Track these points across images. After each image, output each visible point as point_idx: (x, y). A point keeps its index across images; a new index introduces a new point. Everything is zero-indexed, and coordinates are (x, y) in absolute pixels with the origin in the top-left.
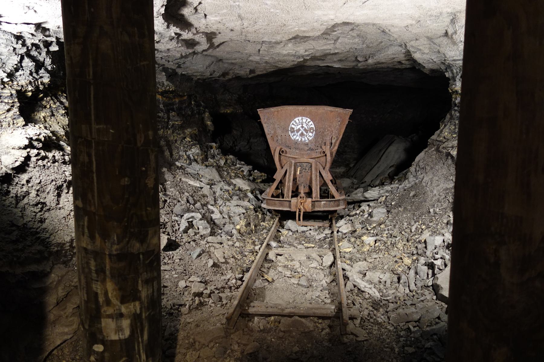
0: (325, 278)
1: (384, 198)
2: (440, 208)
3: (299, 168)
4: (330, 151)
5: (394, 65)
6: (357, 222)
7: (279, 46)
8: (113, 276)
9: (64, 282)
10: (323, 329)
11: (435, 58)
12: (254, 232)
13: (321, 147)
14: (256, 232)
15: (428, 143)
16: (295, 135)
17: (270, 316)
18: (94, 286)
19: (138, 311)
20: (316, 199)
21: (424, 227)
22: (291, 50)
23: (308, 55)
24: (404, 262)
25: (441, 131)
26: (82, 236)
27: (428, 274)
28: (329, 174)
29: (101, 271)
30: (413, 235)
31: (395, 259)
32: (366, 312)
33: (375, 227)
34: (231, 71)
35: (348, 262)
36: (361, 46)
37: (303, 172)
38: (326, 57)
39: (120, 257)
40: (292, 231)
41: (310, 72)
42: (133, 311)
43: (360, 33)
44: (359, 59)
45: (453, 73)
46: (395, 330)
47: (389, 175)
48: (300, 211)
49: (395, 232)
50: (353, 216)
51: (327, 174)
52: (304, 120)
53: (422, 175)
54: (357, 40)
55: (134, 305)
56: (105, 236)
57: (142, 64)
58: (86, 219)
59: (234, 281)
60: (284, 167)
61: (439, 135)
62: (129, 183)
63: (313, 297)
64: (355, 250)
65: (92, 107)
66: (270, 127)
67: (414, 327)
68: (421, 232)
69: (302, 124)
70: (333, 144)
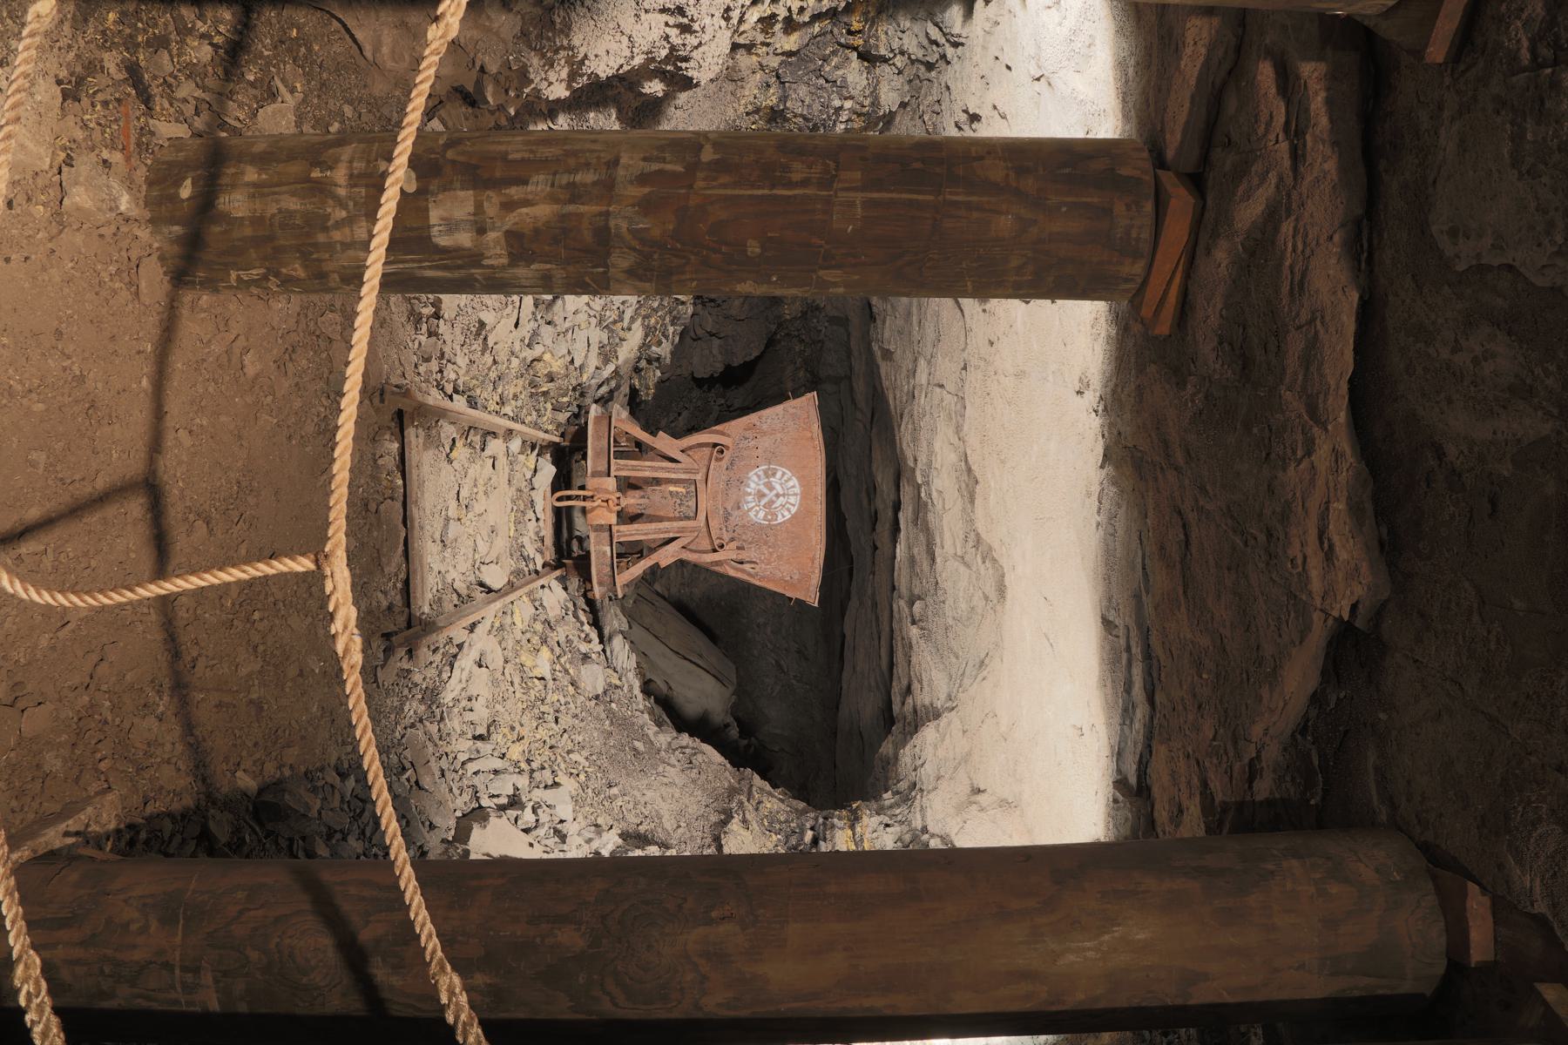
1: (618, 683)
2: (623, 808)
3: (684, 490)
4: (726, 561)
5: (899, 678)
8: (563, 217)
9: (484, 39)
10: (385, 593)
11: (928, 771)
12: (533, 390)
13: (732, 540)
15: (742, 769)
16: (760, 479)
17: (404, 478)
18: (542, 177)
19: (485, 262)
20: (615, 535)
21: (582, 777)
24: (513, 746)
25: (770, 794)
26: (642, 155)
27: (498, 796)
29: (575, 194)
30: (563, 758)
31: (517, 725)
32: (417, 678)
33: (567, 671)
34: (889, 306)
35: (497, 625)
36: (950, 614)
38: (922, 531)
39: (604, 236)
41: (879, 480)
42: (488, 254)
44: (918, 606)
45: (891, 807)
46: (395, 741)
48: (585, 498)
49: (566, 720)
51: (673, 556)
52: (792, 500)
53: (676, 763)
55: (500, 256)
56: (647, 206)
57: (969, 283)
58: (679, 168)
59: (453, 376)
60: (684, 455)
61: (762, 790)
62: (749, 253)
64: (519, 636)
65: (894, 195)
66: (775, 421)
67: (408, 780)
68: (571, 774)
69: (784, 495)
70: (740, 566)
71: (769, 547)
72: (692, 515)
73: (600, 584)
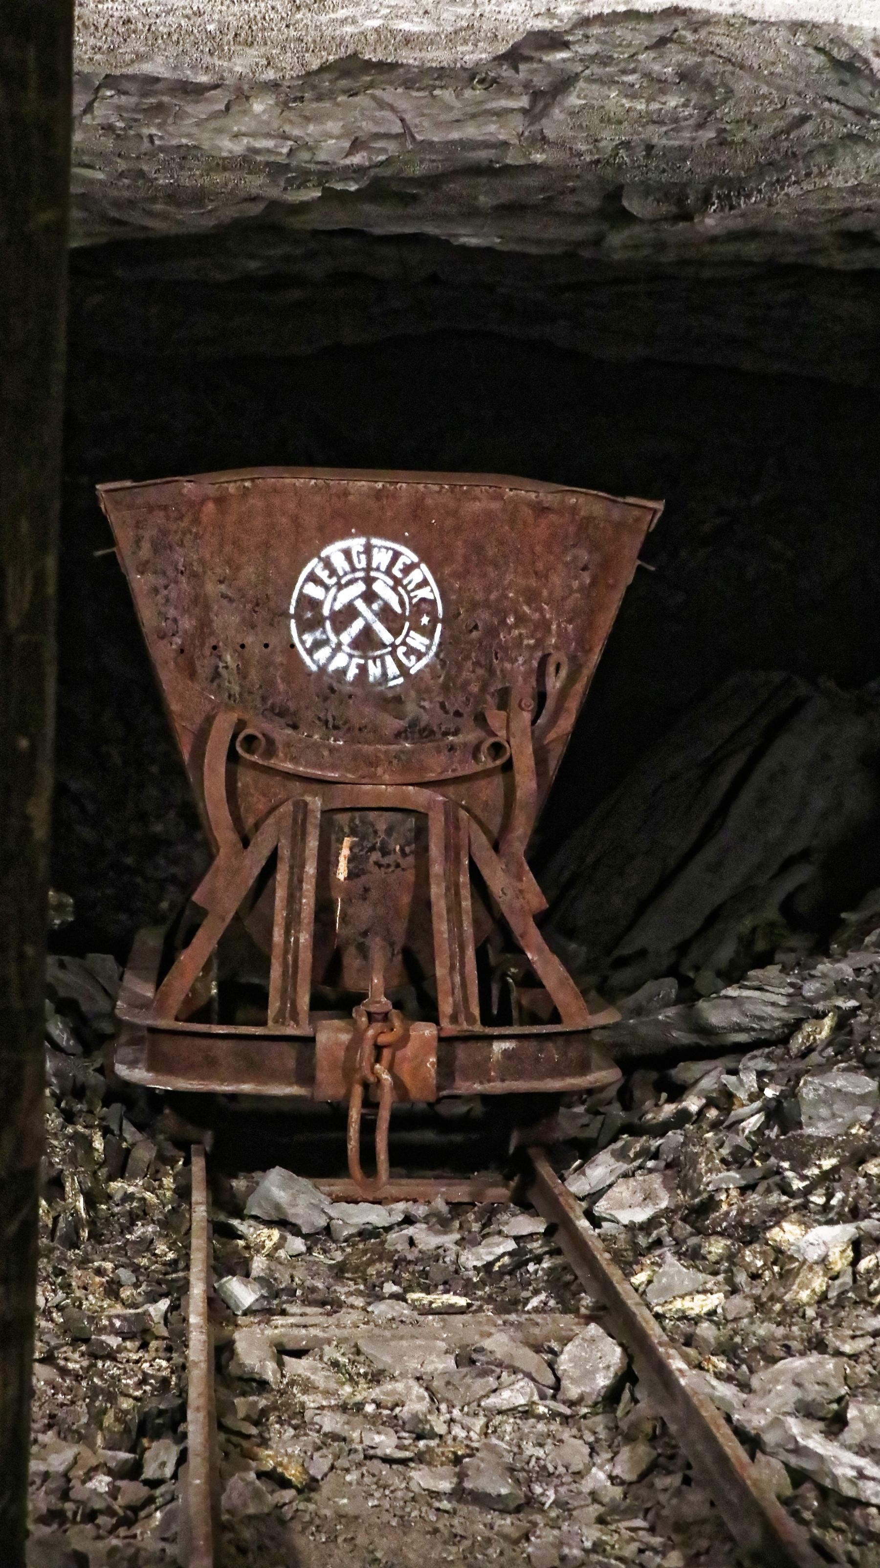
0: (598, 1460)
1: (828, 1022)
3: (347, 841)
6: (710, 1158)
7: (198, 110)
13: (481, 720)
14: (96, 1237)
16: (326, 642)
22: (268, 136)
23: (359, 171)
28: (529, 878)
33: (827, 1177)
37: (370, 866)
40: (296, 1231)
43: (699, 65)
47: (786, 907)
48: (370, 1104)
50: (661, 1130)
52: (381, 558)
54: (673, 102)
59: (101, 1483)
63: (566, 1550)
64: (741, 1304)
66: (173, 595)
69: (369, 581)
70: (550, 703)
71: (503, 622)
72: (411, 822)
73: (584, 1068)
